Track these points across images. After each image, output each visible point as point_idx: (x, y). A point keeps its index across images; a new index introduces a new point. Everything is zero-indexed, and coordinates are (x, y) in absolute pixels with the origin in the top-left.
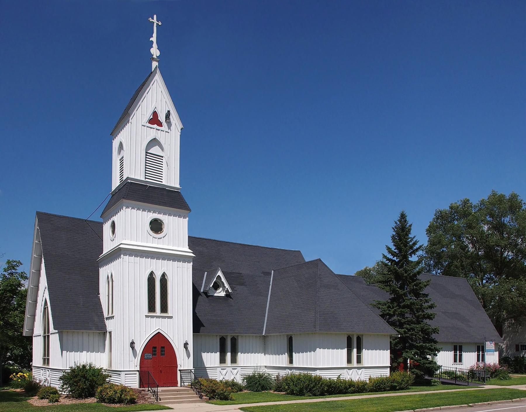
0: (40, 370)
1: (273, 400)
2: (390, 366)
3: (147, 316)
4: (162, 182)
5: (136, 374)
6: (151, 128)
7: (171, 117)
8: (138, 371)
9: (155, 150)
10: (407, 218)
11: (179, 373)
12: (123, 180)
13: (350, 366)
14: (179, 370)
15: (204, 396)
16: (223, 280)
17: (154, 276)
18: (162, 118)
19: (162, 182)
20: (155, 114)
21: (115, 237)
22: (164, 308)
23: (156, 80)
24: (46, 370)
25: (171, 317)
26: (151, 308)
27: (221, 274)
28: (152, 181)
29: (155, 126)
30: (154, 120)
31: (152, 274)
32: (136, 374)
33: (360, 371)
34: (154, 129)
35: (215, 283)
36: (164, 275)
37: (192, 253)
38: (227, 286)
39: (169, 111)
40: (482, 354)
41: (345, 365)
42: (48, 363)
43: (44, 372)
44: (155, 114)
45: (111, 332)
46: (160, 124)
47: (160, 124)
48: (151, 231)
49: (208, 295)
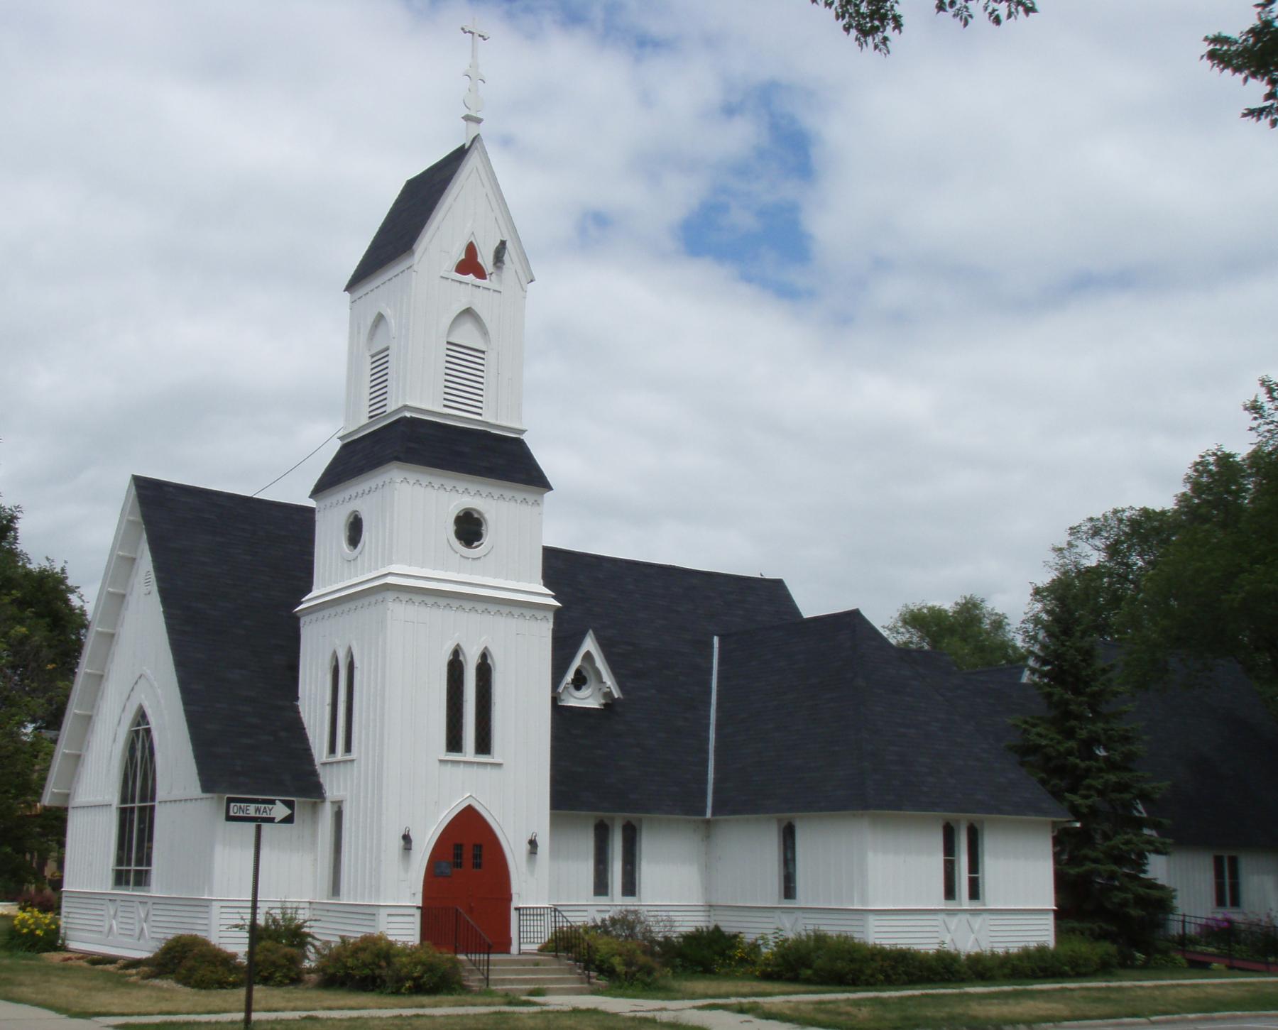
0: (102, 902)
1: (292, 1005)
2: (1054, 911)
3: (441, 761)
4: (480, 415)
5: (413, 915)
6: (461, 282)
7: (506, 258)
8: (418, 908)
9: (467, 335)
10: (1095, 516)
11: (514, 914)
12: (385, 412)
13: (951, 905)
14: (516, 909)
15: (594, 977)
16: (600, 663)
17: (461, 658)
18: (485, 258)
19: (480, 415)
20: (471, 250)
21: (360, 553)
22: (484, 745)
23: (475, 169)
24: (103, 905)
25: (500, 765)
26: (454, 743)
27: (593, 648)
28: (459, 416)
29: (470, 278)
30: (469, 265)
31: (457, 652)
32: (413, 915)
33: (977, 922)
34: (468, 284)
35: (578, 672)
36: (484, 656)
37: (553, 597)
38: (609, 680)
39: (503, 243)
40: (146, 806)
41: (938, 901)
42: (142, 879)
43: (120, 909)
44: (471, 250)
45: (342, 801)
46: (480, 274)
47: (480, 274)
48: (456, 540)
49: (560, 704)
